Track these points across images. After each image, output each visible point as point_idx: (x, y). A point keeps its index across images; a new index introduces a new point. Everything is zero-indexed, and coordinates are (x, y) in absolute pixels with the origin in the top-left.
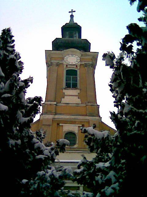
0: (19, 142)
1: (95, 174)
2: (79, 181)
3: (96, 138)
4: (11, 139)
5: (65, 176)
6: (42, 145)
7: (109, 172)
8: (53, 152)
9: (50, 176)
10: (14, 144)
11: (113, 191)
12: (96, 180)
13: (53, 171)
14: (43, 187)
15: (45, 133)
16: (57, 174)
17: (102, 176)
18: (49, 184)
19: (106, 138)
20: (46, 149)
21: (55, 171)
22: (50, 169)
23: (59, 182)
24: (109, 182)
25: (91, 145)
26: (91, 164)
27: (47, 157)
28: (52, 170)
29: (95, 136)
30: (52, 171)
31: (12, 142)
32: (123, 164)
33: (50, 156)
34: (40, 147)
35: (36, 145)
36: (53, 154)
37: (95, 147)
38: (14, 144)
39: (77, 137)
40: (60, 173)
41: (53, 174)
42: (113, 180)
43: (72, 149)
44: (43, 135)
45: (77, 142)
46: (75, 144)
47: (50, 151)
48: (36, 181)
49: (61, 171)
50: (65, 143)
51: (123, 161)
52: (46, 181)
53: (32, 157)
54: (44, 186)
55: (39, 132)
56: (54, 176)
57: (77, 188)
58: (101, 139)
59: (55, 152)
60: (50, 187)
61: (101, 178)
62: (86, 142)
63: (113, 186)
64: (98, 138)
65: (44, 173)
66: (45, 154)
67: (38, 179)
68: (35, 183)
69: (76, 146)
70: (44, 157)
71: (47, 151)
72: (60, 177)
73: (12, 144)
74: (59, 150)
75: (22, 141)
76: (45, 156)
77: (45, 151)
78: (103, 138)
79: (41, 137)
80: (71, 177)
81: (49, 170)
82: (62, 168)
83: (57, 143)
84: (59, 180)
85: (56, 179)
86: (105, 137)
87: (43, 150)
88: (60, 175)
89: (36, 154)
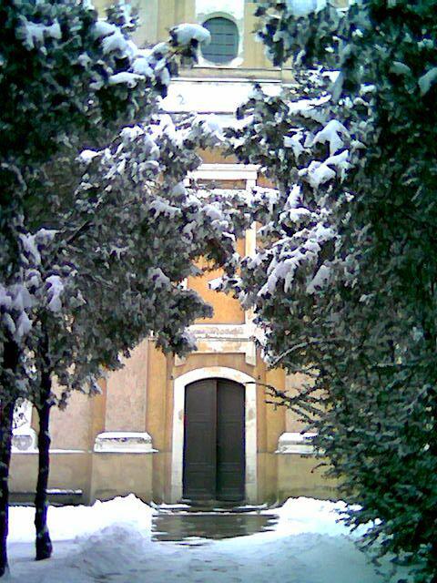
0: (55, 30)
1: (286, 128)
2: (242, 155)
3: (291, 17)
4: (31, 23)
5: (199, 143)
6: (131, 49)
7: (324, 123)
8: (161, 64)
9: (159, 142)
10: (40, 37)
11: (331, 173)
12: (286, 145)
13: (140, 57)
14: (141, 169)
15: (134, 12)
16: (178, 138)
17: (305, 136)
18: (156, 164)
19: (320, 12)
20: (140, 57)
21: (171, 128)
22: (158, 122)
23: (183, 157)
24: (322, 151)
25: (275, 38)
26: (275, 107)
27: (143, 77)
28: (162, 124)
29: (289, 9)
30: (162, 129)
31: (33, 31)
32: (366, 97)
33: (153, 77)
34: (121, 49)
35: (107, 44)
36: (162, 70)
37: (286, 45)
38: (40, 37)
39: (241, 34)
40: (186, 134)
41: (166, 136)
42: (336, 143)
43: (225, 72)
44: (128, 19)
45: (240, 50)
46: (232, 56)
47: (152, 62)
48: (120, 155)
49: (190, 129)
50: (194, 37)
51: (365, 89)
52: (148, 155)
53: (98, 77)
54: (143, 166)
55: (116, 10)
56: (170, 141)
57: (239, 184)
58: (306, 17)
59: (167, 65)
60: (159, 170)
61: (302, 142)
62: (261, 34)
63: (332, 159)
64: (297, 16)
65: (141, 132)
66: (136, 70)
67: (124, 151)
68: (117, 160)
69: (235, 63)
70: (136, 80)
71: (142, 64)
72: (188, 144)
73: (34, 38)
74: (177, 59)
75: (64, 28)
76: (137, 76)
77: (136, 62)
78: (311, 15)
79: (123, 26)
80: (217, 144)
81: (153, 127)
82: (192, 118)
83: (171, 38)
84: (185, 152)
85: (177, 150)
86: (317, 11)
87: (131, 58)
88: (185, 138)
89: (109, 70)
